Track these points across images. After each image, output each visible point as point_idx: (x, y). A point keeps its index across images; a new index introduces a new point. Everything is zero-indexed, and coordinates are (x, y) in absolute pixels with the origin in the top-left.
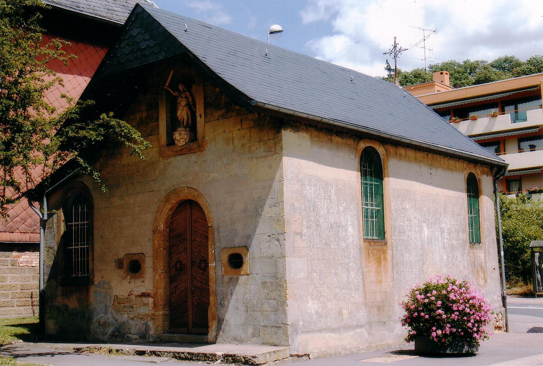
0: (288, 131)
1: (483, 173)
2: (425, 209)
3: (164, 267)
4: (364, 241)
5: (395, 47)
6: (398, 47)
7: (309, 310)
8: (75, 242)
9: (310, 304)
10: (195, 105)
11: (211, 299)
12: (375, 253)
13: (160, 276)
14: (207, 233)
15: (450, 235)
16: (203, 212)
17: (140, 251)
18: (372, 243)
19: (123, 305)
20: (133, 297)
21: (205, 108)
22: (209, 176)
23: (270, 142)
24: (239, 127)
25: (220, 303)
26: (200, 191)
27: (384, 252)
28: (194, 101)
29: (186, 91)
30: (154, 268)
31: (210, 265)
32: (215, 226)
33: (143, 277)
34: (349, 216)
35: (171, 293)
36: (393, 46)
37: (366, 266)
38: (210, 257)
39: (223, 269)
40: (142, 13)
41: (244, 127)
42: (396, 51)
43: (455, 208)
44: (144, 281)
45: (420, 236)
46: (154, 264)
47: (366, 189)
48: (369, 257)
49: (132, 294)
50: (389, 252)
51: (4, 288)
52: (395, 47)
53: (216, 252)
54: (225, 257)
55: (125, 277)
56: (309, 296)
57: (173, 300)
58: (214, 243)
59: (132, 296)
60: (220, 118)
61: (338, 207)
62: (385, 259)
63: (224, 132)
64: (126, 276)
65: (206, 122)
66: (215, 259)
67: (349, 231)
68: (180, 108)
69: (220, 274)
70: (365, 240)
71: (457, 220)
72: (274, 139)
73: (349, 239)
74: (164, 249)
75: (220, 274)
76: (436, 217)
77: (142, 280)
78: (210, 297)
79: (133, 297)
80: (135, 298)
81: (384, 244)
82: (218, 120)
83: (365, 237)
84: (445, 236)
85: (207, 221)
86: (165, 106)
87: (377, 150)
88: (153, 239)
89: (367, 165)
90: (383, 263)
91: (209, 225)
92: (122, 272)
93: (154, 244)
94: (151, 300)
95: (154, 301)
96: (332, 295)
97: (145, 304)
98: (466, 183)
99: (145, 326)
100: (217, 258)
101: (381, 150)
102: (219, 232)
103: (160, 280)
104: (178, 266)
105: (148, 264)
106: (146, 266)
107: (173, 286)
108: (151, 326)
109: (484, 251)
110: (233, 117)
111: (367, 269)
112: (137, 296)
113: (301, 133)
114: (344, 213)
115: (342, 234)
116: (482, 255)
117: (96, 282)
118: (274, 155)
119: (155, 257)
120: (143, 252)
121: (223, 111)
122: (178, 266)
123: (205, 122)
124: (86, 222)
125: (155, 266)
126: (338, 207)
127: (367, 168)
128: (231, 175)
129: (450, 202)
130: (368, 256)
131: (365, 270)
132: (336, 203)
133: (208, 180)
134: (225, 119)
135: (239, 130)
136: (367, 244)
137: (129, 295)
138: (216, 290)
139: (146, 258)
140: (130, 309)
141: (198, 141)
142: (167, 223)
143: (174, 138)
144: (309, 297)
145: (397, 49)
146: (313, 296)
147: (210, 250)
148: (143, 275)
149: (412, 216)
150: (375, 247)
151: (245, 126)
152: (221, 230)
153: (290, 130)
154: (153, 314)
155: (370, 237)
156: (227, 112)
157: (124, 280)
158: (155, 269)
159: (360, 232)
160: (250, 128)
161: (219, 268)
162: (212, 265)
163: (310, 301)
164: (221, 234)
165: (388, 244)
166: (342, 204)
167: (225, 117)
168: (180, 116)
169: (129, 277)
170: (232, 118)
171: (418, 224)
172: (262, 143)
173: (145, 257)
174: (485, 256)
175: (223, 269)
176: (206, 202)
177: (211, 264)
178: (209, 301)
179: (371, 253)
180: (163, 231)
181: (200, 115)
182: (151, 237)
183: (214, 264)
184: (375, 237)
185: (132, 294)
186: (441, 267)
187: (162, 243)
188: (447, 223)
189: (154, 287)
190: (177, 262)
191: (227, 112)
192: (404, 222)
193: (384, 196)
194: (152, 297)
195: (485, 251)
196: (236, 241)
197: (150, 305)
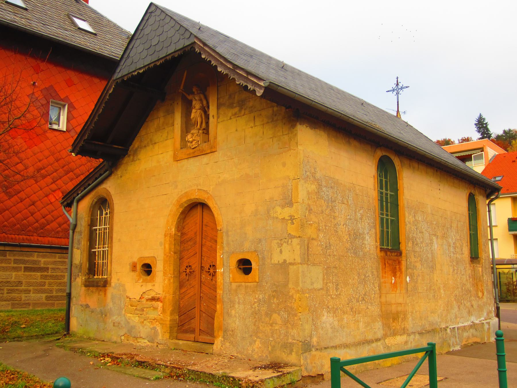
0: (304, 126)
1: (480, 194)
2: (435, 223)
3: (174, 270)
4: (381, 251)
5: (397, 85)
6: (395, 93)
7: (324, 325)
8: (99, 245)
9: (325, 317)
10: (208, 107)
11: (218, 306)
12: (391, 264)
13: (169, 280)
14: (217, 236)
15: (455, 249)
16: (213, 215)
17: (152, 255)
18: (388, 253)
19: (135, 308)
20: (144, 300)
21: (218, 108)
22: (219, 177)
23: (284, 138)
24: (252, 125)
25: (227, 312)
26: (210, 193)
27: (399, 263)
28: (208, 103)
29: (201, 93)
30: (164, 272)
31: (217, 270)
32: (225, 230)
33: (154, 281)
34: (367, 224)
35: (180, 298)
36: (395, 85)
37: (383, 277)
38: (218, 262)
39: (231, 275)
40: (155, 11)
41: (257, 124)
42: (397, 89)
43: (459, 224)
44: (154, 285)
45: (431, 248)
46: (164, 268)
47: (382, 197)
48: (385, 267)
49: (143, 298)
50: (403, 263)
51: (61, 285)
52: (397, 85)
53: (224, 257)
54: (233, 263)
55: (138, 281)
56: (324, 308)
57: (181, 306)
58: (222, 248)
59: (143, 299)
60: (232, 117)
61: (355, 213)
62: (400, 269)
63: (237, 130)
64: (139, 280)
65: (219, 122)
66: (223, 265)
67: (366, 239)
68: (194, 111)
69: (227, 280)
70: (382, 249)
71: (461, 236)
72: (289, 134)
73: (366, 248)
74: (175, 253)
75: (227, 280)
76: (444, 231)
77: (153, 284)
78: (217, 305)
79: (144, 300)
80: (146, 302)
81: (399, 254)
82: (231, 119)
83: (381, 247)
84: (451, 250)
85: (216, 224)
86: (180, 110)
87: (393, 160)
88: (164, 243)
89: (382, 175)
90: (398, 274)
91: (219, 228)
92: (134, 275)
93: (165, 248)
94: (160, 304)
95: (163, 306)
96: (348, 307)
97: (155, 309)
98: (467, 201)
99: (153, 331)
100: (225, 264)
101: (396, 161)
102: (228, 236)
103: (170, 284)
104: (188, 271)
105: (159, 268)
106: (157, 269)
107: (183, 290)
108: (159, 331)
109: (481, 265)
110: (247, 114)
111: (384, 280)
112: (147, 300)
113: (318, 130)
114: (362, 220)
115: (359, 242)
116: (480, 269)
117: (113, 284)
118: (288, 151)
119: (165, 262)
120: (155, 256)
121: (236, 110)
122: (188, 271)
123: (218, 123)
124: (108, 226)
125: (165, 270)
126: (355, 213)
127: (382, 178)
128: (242, 175)
129: (455, 218)
130: (384, 266)
131: (382, 280)
132: (354, 209)
133: (218, 181)
134: (238, 118)
135: (252, 127)
136: (383, 254)
137: (140, 298)
138: (223, 298)
139: (157, 261)
140: (141, 312)
141: (211, 142)
142: (178, 227)
143: (187, 140)
144: (325, 309)
145: (399, 87)
146: (328, 308)
147: (218, 254)
148: (154, 279)
149: (424, 228)
150: (391, 257)
151: (257, 123)
152: (230, 233)
153: (307, 125)
154: (162, 319)
155: (385, 247)
156: (240, 111)
157: (137, 284)
158: (165, 274)
159: (376, 241)
160: (263, 124)
161: (227, 274)
162: (220, 270)
163: (326, 314)
164: (230, 238)
165: (403, 255)
166: (359, 211)
167: (238, 116)
168: (193, 118)
169: (141, 281)
170: (244, 116)
171: (429, 236)
172: (275, 139)
173: (156, 261)
174: (482, 270)
175: (231, 275)
176: (216, 204)
177: (219, 269)
178: (216, 308)
179: (387, 263)
180: (175, 234)
181: (213, 116)
182: (163, 240)
183: (222, 270)
184: (390, 248)
185: (143, 298)
186: (448, 279)
187: (173, 247)
188: (452, 237)
189: (163, 291)
190: (187, 267)
191: (240, 111)
192: (417, 234)
193: (399, 207)
194: (161, 302)
195: (482, 266)
196: (245, 246)
197: (159, 310)
